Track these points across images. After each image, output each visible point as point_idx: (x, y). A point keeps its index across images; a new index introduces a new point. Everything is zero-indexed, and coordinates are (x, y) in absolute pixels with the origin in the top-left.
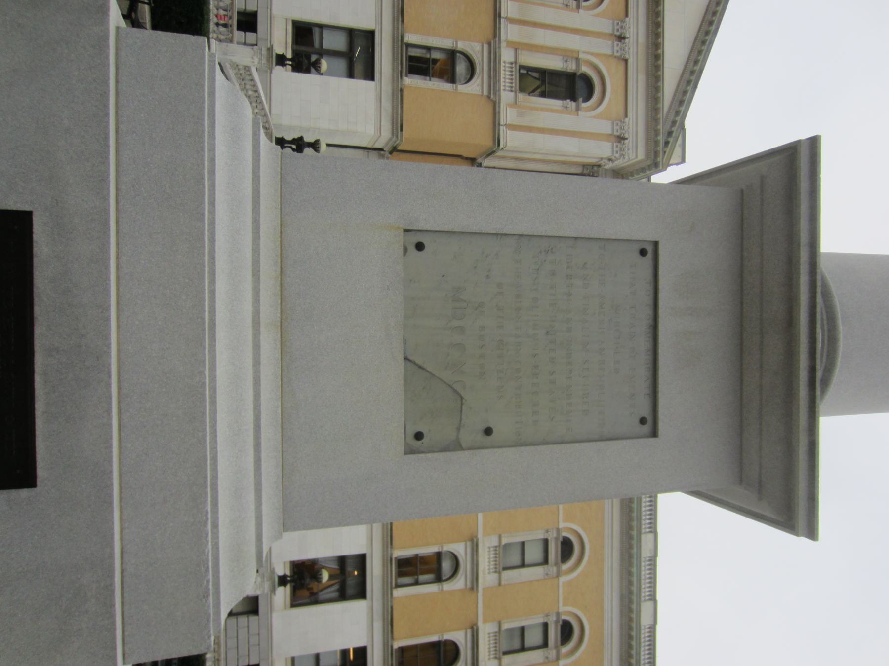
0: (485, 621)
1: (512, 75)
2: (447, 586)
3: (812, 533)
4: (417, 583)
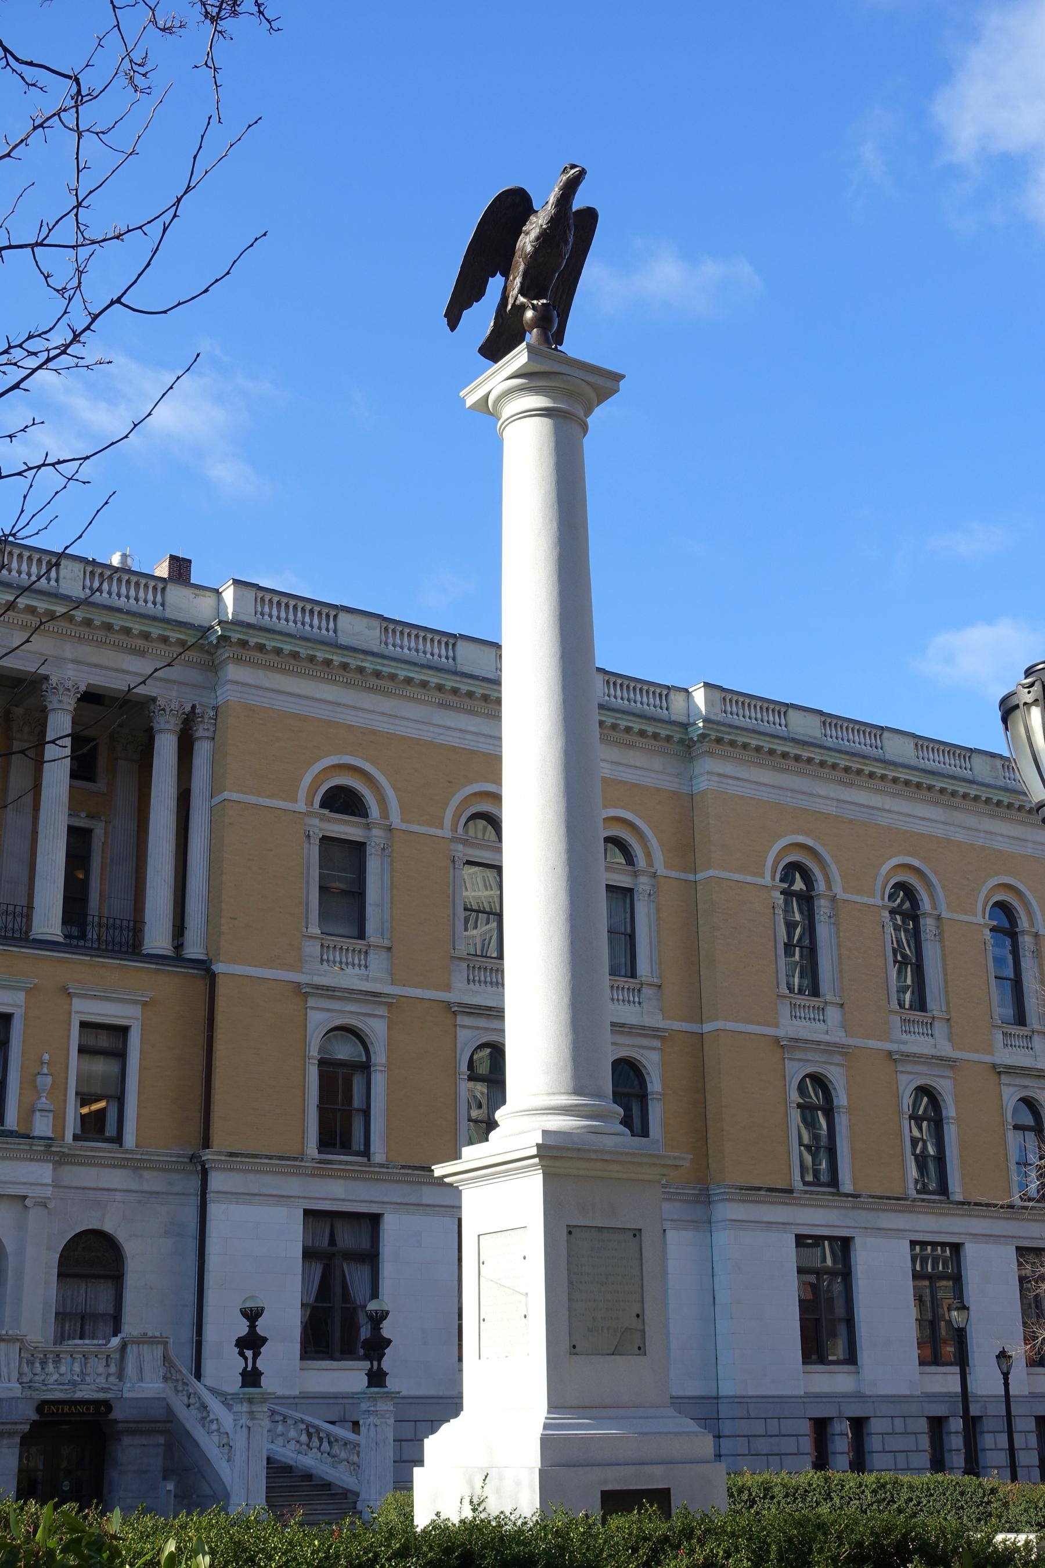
0: (448, 987)
1: (354, 951)
2: (379, 1057)
3: (618, 377)
4: (366, 1113)
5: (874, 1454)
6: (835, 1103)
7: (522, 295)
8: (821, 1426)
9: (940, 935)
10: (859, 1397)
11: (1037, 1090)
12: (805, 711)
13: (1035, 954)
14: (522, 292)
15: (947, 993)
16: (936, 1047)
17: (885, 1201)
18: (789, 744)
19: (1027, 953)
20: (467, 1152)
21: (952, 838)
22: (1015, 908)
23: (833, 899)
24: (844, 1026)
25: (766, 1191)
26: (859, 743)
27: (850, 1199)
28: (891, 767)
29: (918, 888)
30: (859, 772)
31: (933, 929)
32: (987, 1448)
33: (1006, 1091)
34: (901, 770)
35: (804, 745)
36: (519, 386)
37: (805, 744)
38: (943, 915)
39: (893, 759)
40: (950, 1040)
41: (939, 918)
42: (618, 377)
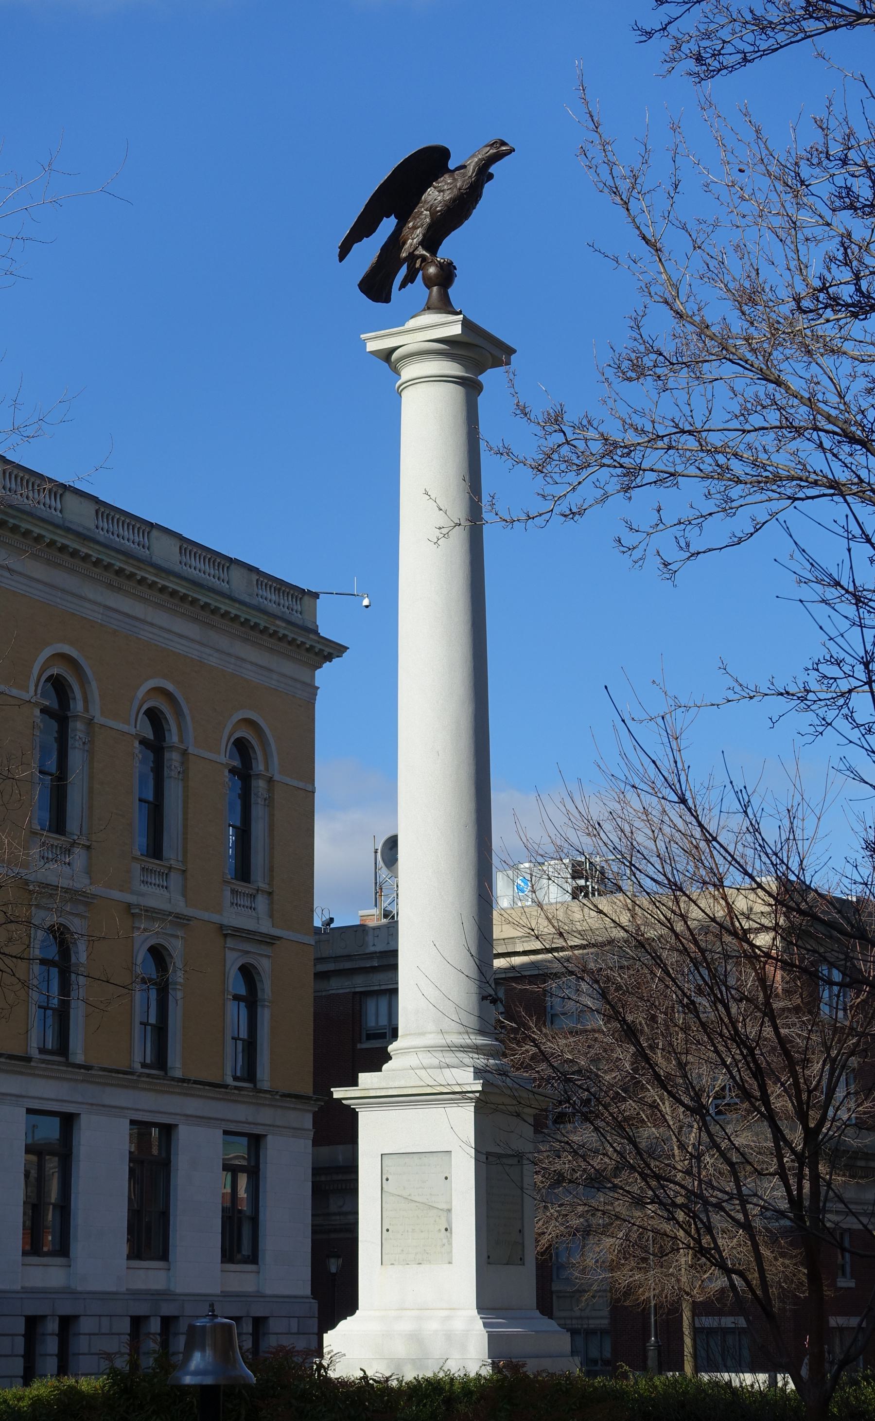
5: (81, 1356)
6: (73, 960)
7: (423, 247)
8: (33, 1323)
9: (185, 774)
10: (69, 1292)
11: (258, 958)
12: (81, 496)
13: (267, 802)
14: (422, 243)
15: (185, 839)
16: (170, 903)
17: (114, 1075)
18: (70, 536)
19: (259, 800)
20: (364, 1078)
21: (206, 661)
22: (253, 748)
23: (90, 722)
24: (89, 871)
25: (6, 1058)
26: (128, 540)
27: (82, 1071)
28: (163, 575)
29: (168, 716)
30: (131, 576)
31: (177, 764)
32: (81, 1352)
33: (231, 956)
34: (172, 578)
35: (84, 539)
36: (443, 350)
37: (78, 534)
38: (190, 750)
39: (160, 562)
40: (184, 894)
41: (184, 753)
42: (511, 351)
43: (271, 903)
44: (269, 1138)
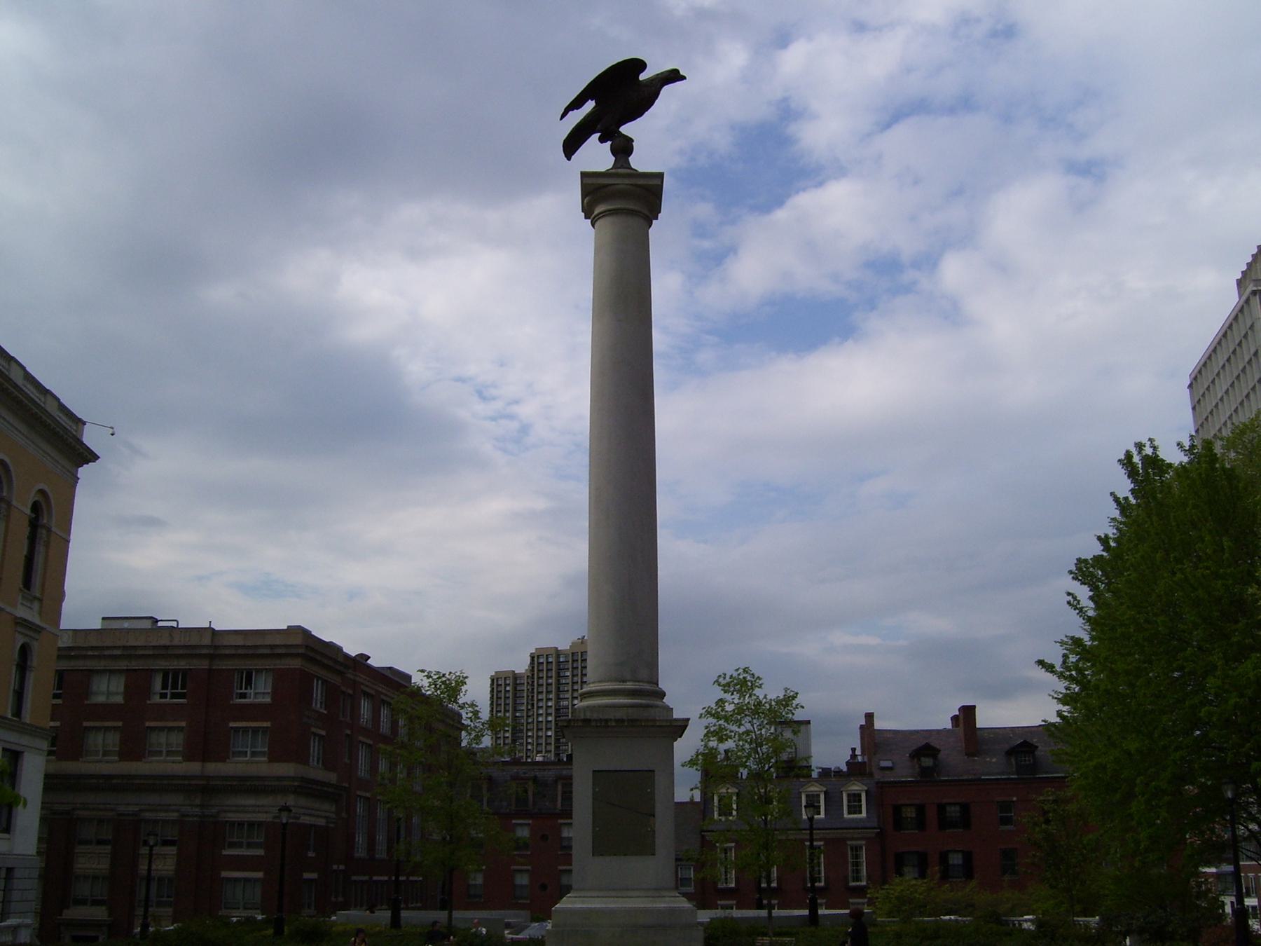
43: (41, 607)
44: (25, 754)
